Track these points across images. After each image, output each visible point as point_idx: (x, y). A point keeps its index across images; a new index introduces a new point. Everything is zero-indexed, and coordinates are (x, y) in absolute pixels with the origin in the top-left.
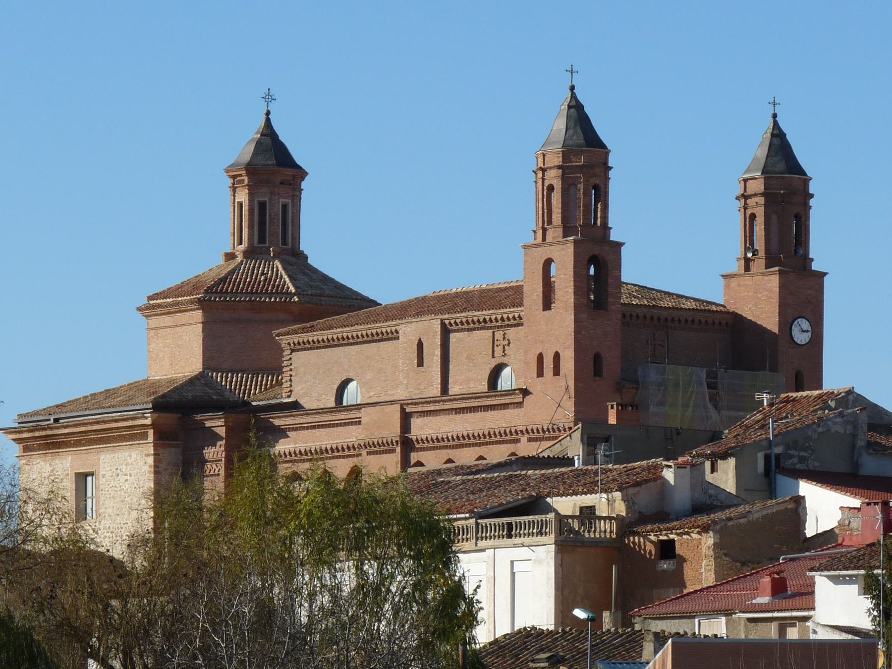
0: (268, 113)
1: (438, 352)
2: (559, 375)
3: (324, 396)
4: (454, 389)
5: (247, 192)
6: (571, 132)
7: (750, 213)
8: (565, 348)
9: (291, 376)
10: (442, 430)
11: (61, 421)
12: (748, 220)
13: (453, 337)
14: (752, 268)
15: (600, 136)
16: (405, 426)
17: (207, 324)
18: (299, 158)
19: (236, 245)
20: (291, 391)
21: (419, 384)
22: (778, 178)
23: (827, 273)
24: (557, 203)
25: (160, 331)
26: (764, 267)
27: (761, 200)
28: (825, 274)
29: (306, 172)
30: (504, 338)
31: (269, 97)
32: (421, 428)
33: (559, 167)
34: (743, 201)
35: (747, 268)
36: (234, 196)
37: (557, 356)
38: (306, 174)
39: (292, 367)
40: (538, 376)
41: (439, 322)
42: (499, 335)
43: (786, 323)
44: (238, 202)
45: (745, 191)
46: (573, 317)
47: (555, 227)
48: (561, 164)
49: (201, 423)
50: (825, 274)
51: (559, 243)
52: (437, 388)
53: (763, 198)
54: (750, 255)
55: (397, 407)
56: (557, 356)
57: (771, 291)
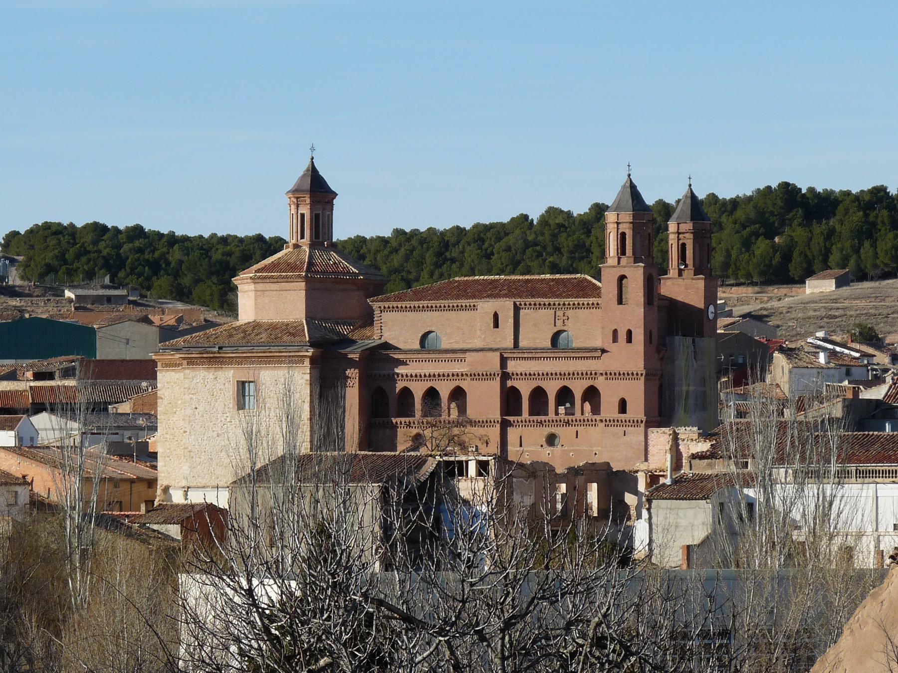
0: (312, 158)
2: (631, 342)
3: (409, 341)
4: (523, 343)
8: (636, 327)
10: (532, 369)
11: (224, 349)
17: (308, 291)
18: (332, 185)
19: (299, 239)
20: (381, 336)
21: (495, 338)
24: (629, 243)
27: (691, 236)
30: (564, 316)
31: (313, 149)
32: (512, 366)
33: (631, 223)
37: (629, 333)
39: (382, 321)
40: (613, 342)
42: (560, 313)
45: (678, 229)
46: (643, 310)
52: (510, 342)
54: (683, 267)
56: (629, 333)
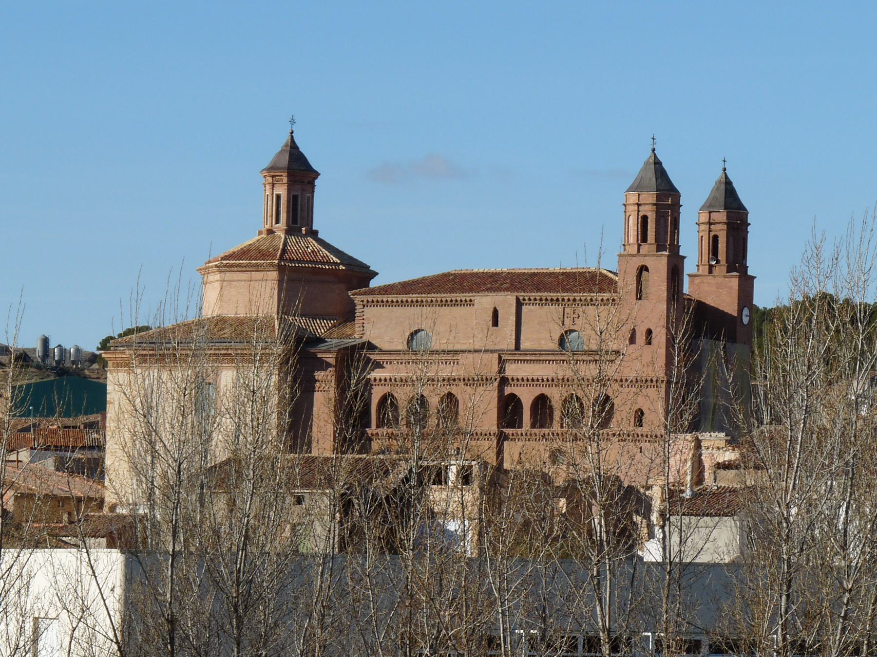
1: (513, 318)
5: (286, 188)
6: (659, 180)
7: (713, 234)
9: (363, 323)
12: (711, 239)
13: (525, 309)
14: (714, 271)
15: (676, 187)
16: (501, 370)
18: (315, 166)
22: (735, 212)
23: (756, 277)
25: (234, 283)
26: (726, 272)
28: (755, 277)
29: (318, 172)
31: (293, 122)
33: (654, 204)
34: (708, 226)
35: (710, 272)
36: (273, 190)
37: (649, 332)
38: (319, 174)
39: (364, 317)
41: (515, 297)
43: (740, 311)
44: (276, 194)
45: (710, 220)
47: (650, 244)
48: (655, 202)
49: (315, 354)
50: (755, 277)
51: (653, 255)
53: (726, 226)
55: (496, 355)
57: (731, 288)
